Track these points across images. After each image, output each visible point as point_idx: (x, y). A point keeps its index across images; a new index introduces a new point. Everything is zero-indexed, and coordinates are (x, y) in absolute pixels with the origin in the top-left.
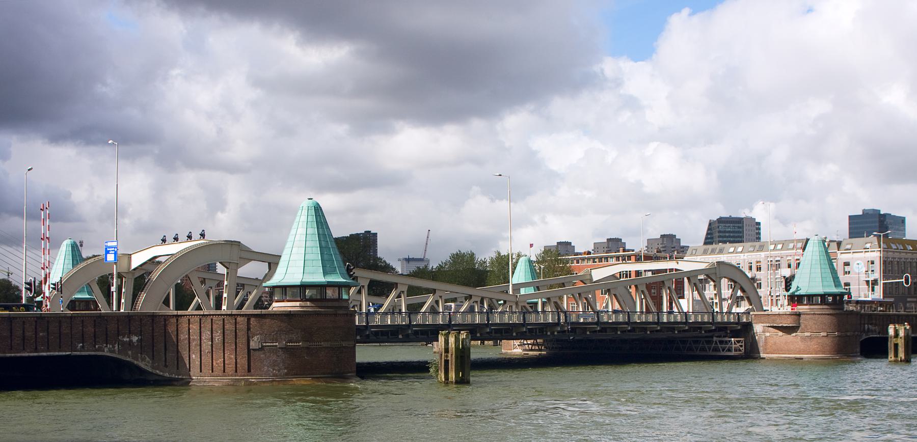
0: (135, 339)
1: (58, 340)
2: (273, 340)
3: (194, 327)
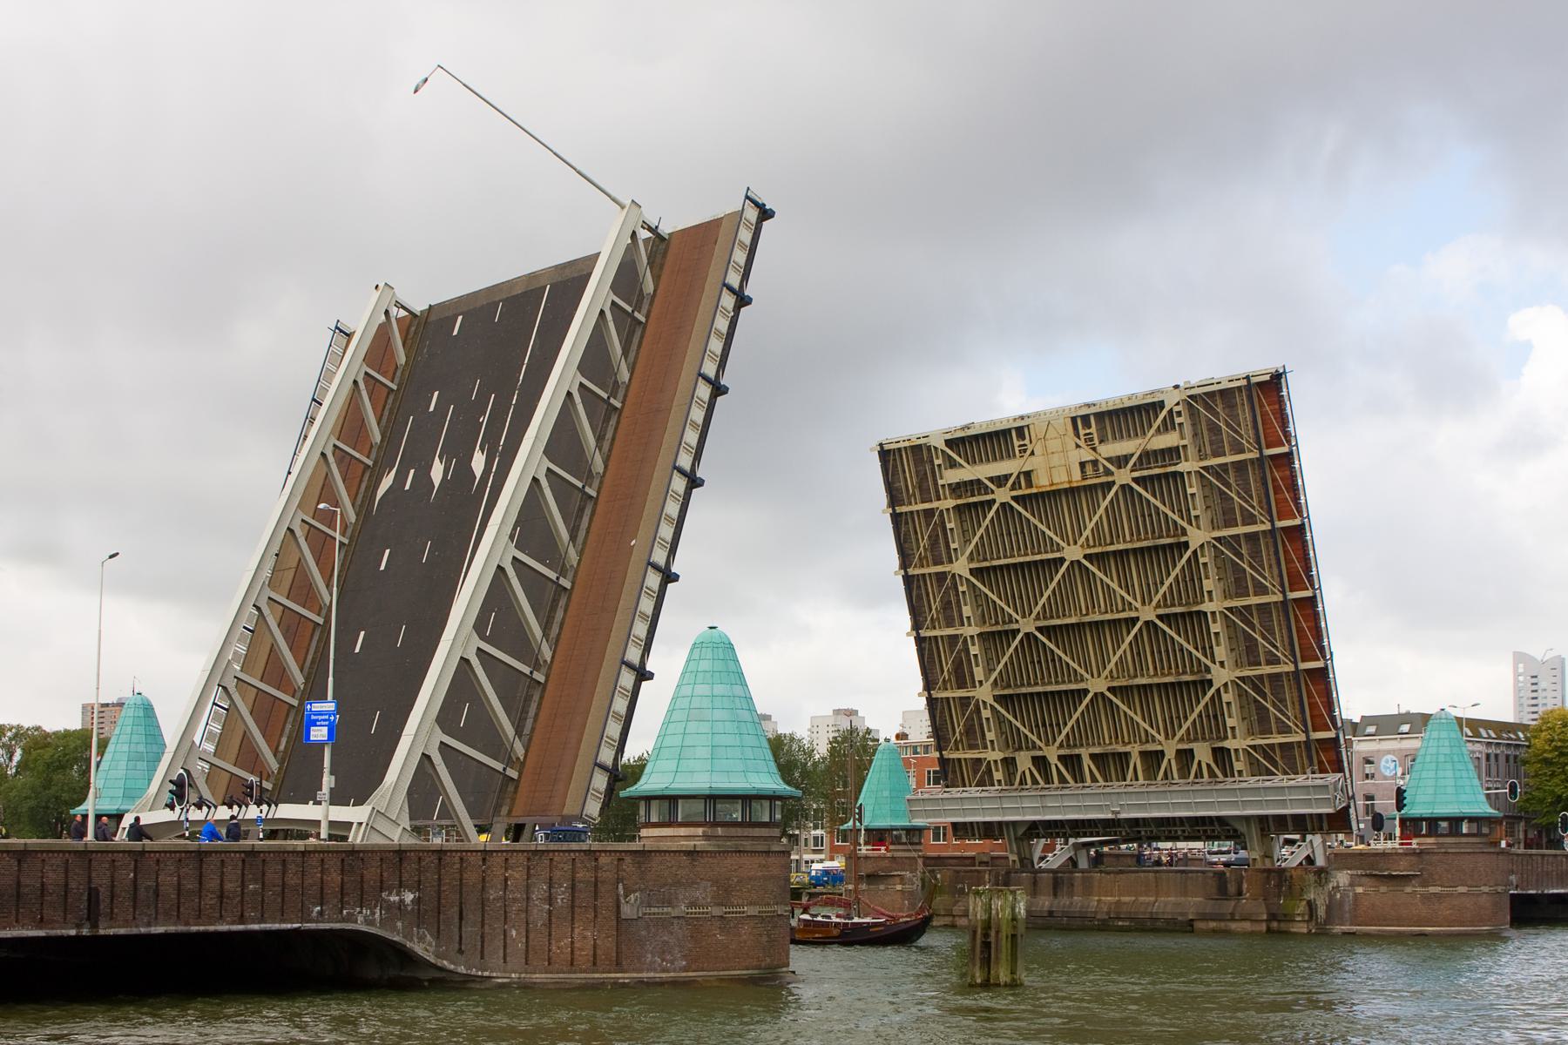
0: (409, 897)
1: (279, 900)
2: (663, 903)
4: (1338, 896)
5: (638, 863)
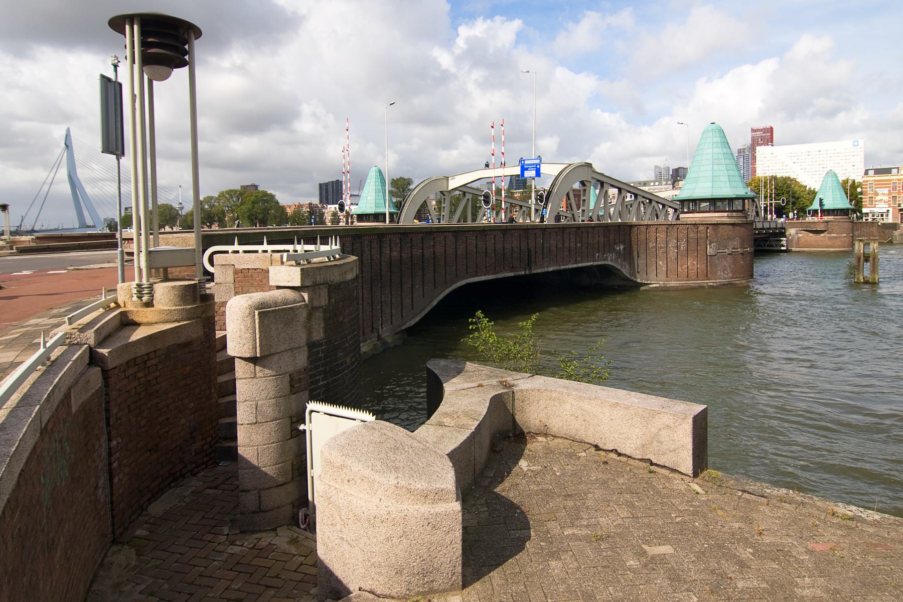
0: (622, 247)
4: (790, 237)
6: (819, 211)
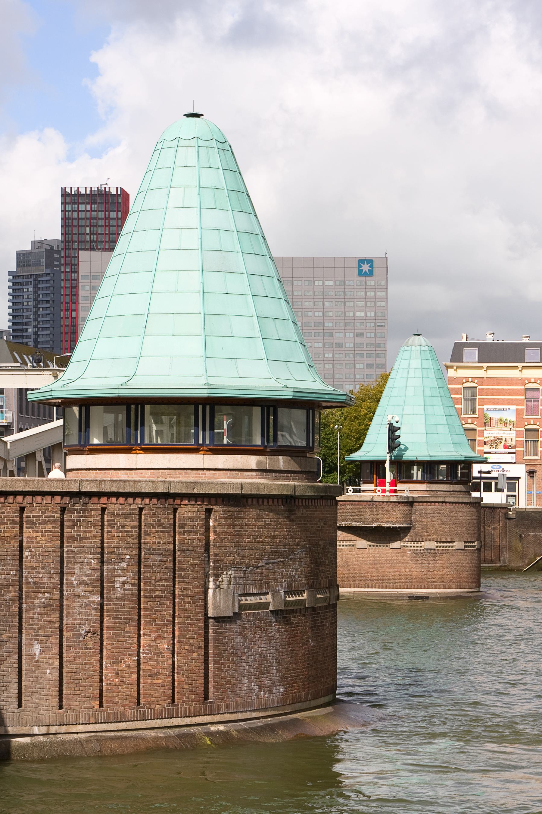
3: (42, 539)
5: (231, 516)
6: (387, 465)
